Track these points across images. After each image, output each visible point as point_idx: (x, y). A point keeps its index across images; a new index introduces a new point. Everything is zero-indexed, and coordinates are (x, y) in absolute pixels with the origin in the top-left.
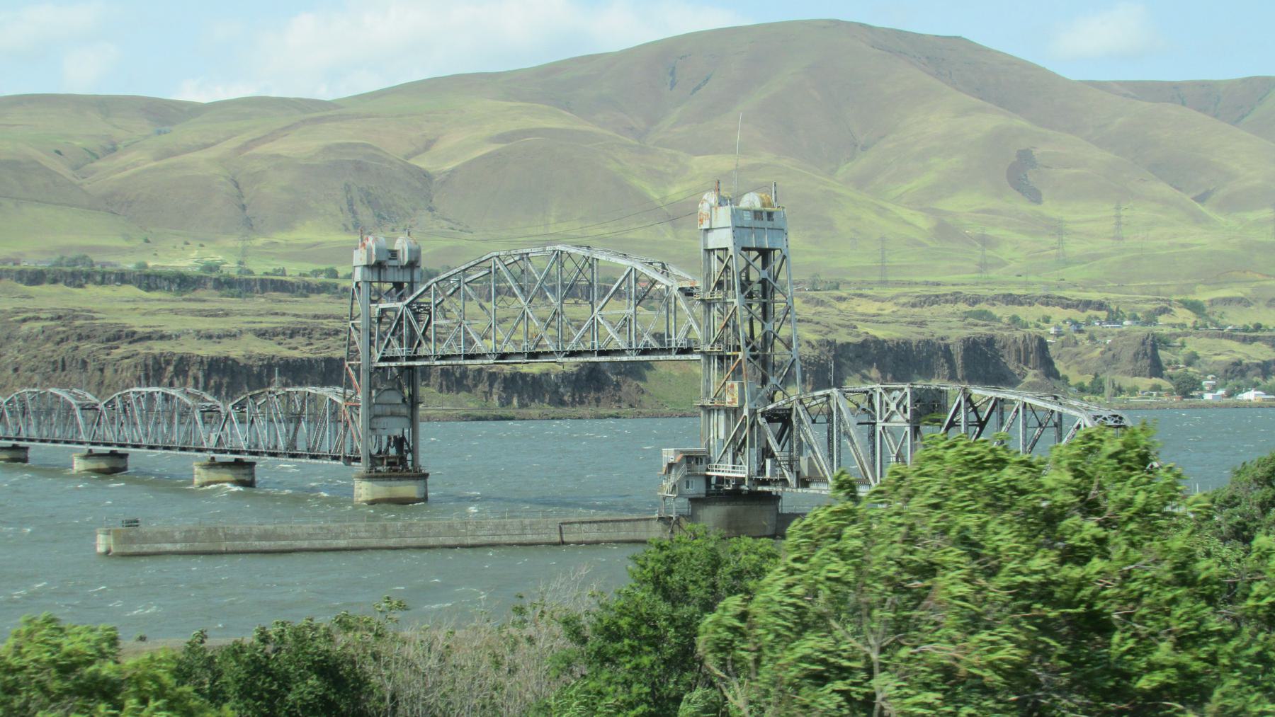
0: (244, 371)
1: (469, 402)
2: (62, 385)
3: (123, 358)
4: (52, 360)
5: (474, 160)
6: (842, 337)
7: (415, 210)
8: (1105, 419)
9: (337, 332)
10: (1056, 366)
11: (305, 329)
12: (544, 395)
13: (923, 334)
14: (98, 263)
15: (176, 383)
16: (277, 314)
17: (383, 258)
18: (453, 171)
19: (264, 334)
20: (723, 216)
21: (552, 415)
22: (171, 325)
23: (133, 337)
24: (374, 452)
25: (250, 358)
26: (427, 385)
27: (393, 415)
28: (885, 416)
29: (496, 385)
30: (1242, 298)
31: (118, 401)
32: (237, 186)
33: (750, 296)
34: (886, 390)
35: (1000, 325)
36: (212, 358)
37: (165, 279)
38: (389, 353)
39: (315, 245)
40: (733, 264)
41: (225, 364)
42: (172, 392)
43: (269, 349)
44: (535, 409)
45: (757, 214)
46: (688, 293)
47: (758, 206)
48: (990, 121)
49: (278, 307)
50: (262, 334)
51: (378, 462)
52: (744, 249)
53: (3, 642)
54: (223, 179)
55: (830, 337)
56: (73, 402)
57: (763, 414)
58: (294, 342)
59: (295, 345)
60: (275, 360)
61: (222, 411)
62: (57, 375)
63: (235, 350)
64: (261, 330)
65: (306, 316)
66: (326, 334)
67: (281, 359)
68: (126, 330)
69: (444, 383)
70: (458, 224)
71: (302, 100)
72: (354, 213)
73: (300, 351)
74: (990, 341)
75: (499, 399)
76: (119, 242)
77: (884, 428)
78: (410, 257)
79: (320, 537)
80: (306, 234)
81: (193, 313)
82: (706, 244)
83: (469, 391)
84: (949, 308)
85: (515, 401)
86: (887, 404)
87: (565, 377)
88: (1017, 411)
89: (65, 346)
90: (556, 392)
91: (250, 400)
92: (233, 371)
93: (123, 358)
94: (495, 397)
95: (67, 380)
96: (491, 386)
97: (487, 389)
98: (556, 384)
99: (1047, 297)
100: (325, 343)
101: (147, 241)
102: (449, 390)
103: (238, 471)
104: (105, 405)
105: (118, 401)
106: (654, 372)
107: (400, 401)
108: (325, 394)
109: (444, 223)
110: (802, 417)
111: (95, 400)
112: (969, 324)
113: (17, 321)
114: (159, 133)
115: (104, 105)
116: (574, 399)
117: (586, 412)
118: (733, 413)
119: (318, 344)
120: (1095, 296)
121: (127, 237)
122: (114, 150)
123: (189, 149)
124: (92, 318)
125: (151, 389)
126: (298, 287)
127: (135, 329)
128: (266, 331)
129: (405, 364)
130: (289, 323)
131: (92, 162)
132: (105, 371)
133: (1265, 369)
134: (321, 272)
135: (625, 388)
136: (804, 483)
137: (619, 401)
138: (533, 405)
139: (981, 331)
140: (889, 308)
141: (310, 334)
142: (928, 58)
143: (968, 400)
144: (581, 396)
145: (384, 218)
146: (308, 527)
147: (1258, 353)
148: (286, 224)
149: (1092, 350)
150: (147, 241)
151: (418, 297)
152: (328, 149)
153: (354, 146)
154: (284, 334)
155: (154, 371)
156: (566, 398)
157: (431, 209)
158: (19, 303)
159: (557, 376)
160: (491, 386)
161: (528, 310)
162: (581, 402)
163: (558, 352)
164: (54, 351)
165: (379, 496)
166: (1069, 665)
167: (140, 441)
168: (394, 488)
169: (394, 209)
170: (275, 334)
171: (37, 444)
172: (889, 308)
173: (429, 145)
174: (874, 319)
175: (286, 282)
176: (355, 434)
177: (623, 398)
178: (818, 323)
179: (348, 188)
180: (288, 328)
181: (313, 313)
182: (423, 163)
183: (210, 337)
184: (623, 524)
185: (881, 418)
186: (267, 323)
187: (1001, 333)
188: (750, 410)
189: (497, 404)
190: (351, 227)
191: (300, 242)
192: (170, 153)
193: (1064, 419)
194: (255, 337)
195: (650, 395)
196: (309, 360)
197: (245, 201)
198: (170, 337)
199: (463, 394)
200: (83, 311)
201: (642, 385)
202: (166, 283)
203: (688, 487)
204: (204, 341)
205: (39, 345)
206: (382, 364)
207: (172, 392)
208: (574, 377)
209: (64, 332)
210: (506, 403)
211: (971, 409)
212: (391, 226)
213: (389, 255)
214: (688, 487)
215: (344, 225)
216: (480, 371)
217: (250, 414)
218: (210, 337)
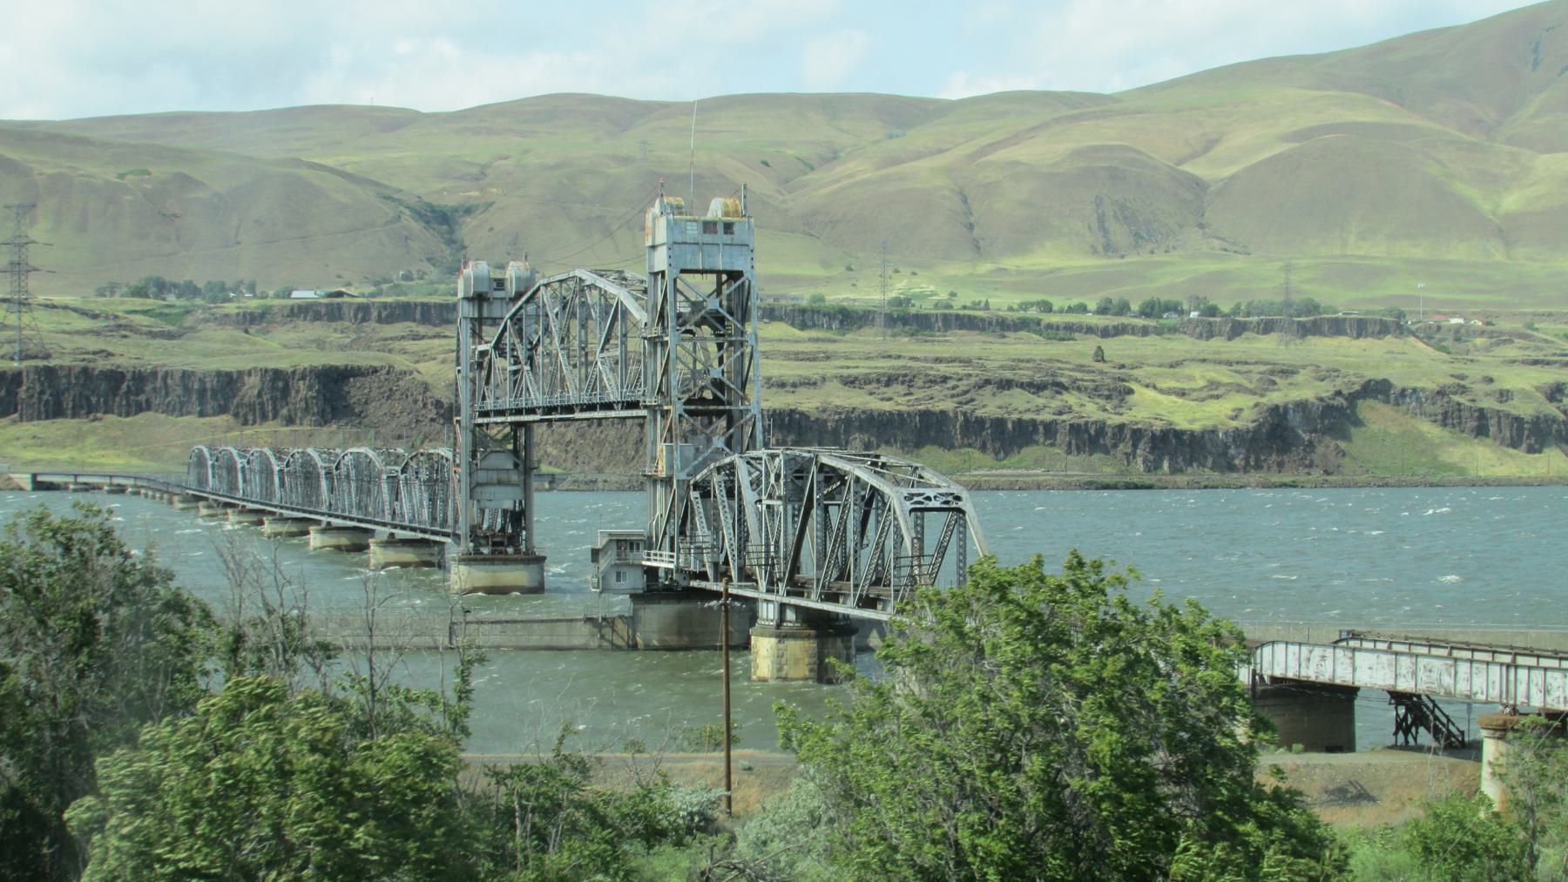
0: (816, 427)
1: (1104, 467)
5: (1259, 164)
7: (1181, 226)
9: (945, 379)
11: (905, 375)
12: (1206, 457)
14: (769, 296)
16: (890, 357)
17: (484, 289)
18: (1233, 178)
19: (852, 382)
21: (1203, 484)
25: (824, 411)
26: (1052, 445)
27: (500, 483)
29: (1141, 445)
32: (965, 201)
36: (774, 411)
37: (824, 315)
39: (1051, 272)
41: (791, 420)
44: (1192, 473)
50: (850, 382)
51: (483, 541)
54: (947, 193)
58: (889, 391)
60: (856, 413)
62: (592, 430)
64: (849, 376)
66: (931, 381)
67: (864, 412)
69: (1073, 442)
70: (1234, 243)
71: (1073, 93)
72: (1105, 231)
73: (896, 402)
75: (1144, 462)
76: (820, 272)
78: (517, 287)
80: (1044, 258)
82: (651, 267)
83: (1107, 452)
85: (1166, 465)
90: (1225, 454)
92: (800, 427)
94: (1140, 460)
95: (603, 436)
96: (1135, 446)
97: (1129, 450)
98: (1225, 444)
100: (929, 392)
101: (850, 269)
102: (1079, 450)
103: (422, 551)
106: (1364, 429)
107: (510, 466)
109: (1216, 243)
114: (891, 137)
115: (831, 106)
116: (1247, 463)
117: (1252, 480)
119: (919, 394)
121: (825, 264)
122: (834, 158)
123: (919, 156)
126: (990, 323)
128: (856, 378)
131: (805, 174)
134: (1032, 304)
135: (1320, 450)
137: (1311, 465)
138: (1190, 470)
141: (911, 381)
144: (1257, 460)
145: (1142, 238)
148: (1019, 248)
150: (850, 269)
152: (1077, 154)
153: (1111, 149)
154: (878, 381)
156: (1237, 462)
157: (1201, 226)
159: (1226, 433)
160: (1135, 446)
162: (1258, 467)
165: (479, 584)
168: (498, 574)
169: (1155, 226)
170: (868, 381)
173: (1210, 144)
175: (975, 317)
179: (1099, 202)
180: (884, 375)
182: (1197, 169)
183: (782, 385)
184: (536, 626)
190: (1100, 248)
191: (1032, 268)
192: (895, 161)
194: (840, 386)
195: (1353, 458)
196: (900, 414)
197: (972, 220)
199: (1097, 456)
201: (1343, 445)
202: (825, 320)
203: (618, 579)
204: (774, 390)
208: (1250, 435)
210: (1152, 467)
212: (1149, 247)
213: (495, 284)
214: (618, 579)
215: (1092, 246)
216: (1121, 427)
218: (782, 385)
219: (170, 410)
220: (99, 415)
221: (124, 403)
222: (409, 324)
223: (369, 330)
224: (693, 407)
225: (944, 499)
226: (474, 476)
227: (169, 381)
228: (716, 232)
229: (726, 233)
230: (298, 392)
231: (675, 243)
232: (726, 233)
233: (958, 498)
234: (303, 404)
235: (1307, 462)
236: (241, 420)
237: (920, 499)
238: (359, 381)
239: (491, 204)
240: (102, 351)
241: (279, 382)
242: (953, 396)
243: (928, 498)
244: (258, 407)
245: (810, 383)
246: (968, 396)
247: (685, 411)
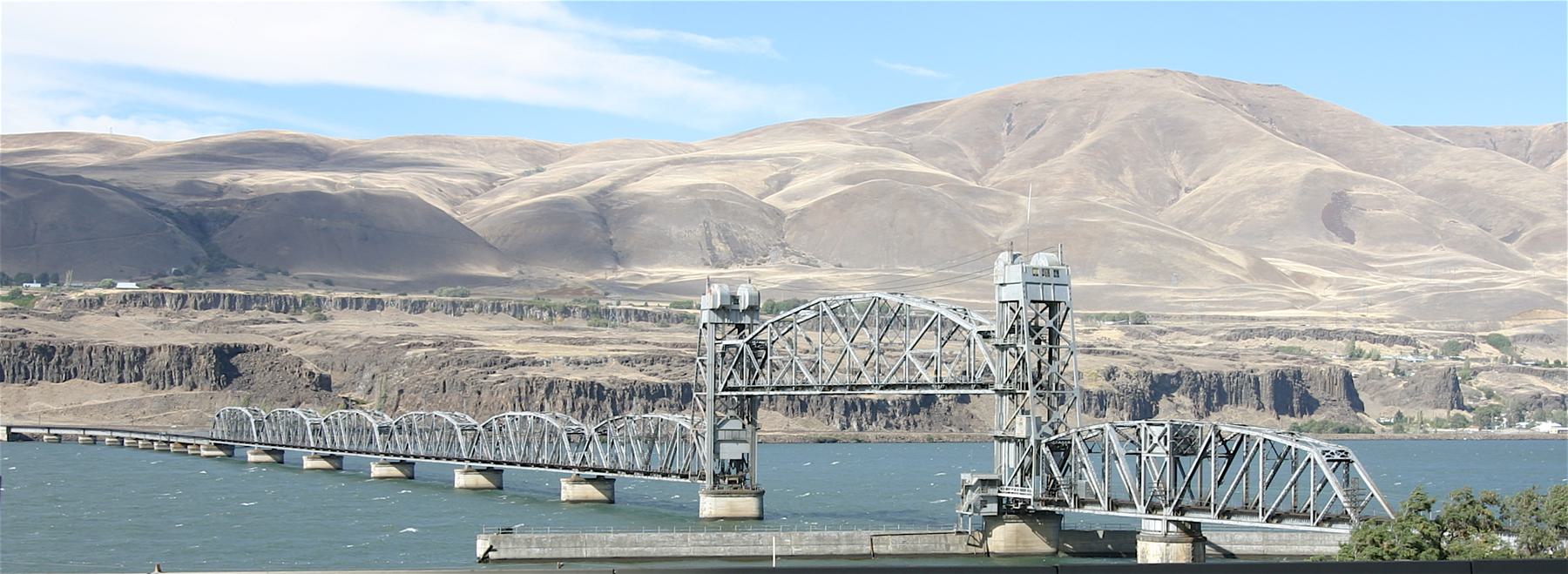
2: (444, 407)
3: (498, 382)
4: (435, 383)
6: (1158, 369)
8: (1332, 453)
10: (1361, 398)
11: (664, 357)
13: (1234, 366)
15: (547, 406)
16: (639, 342)
17: (727, 302)
20: (1015, 273)
23: (508, 363)
24: (717, 472)
28: (1149, 448)
30: (1544, 335)
31: (495, 422)
33: (1038, 342)
34: (1148, 424)
35: (1308, 359)
38: (731, 384)
39: (676, 278)
40: (1023, 314)
42: (542, 416)
43: (631, 375)
45: (1045, 272)
46: (986, 335)
47: (1046, 265)
48: (1301, 166)
49: (639, 336)
50: (626, 361)
52: (1033, 301)
55: (1146, 369)
56: (455, 423)
57: (1046, 444)
59: (655, 372)
60: (637, 385)
61: (586, 433)
63: (601, 376)
65: (666, 345)
67: (643, 384)
68: (501, 357)
73: (654, 377)
74: (1298, 375)
77: (1148, 457)
79: (666, 544)
81: (564, 341)
84: (1262, 342)
85: (854, 425)
86: (1151, 437)
87: (902, 403)
88: (1258, 445)
89: (446, 370)
91: (611, 424)
93: (498, 382)
94: (837, 421)
99: (1356, 332)
100: (683, 369)
104: (483, 427)
105: (495, 422)
108: (676, 420)
109: (794, 258)
110: (1080, 447)
111: (474, 422)
112: (1278, 357)
113: (402, 347)
118: (1021, 442)
119: (676, 371)
120: (1401, 331)
124: (471, 345)
125: (523, 414)
127: (511, 356)
129: (745, 393)
130: (650, 351)
132: (482, 394)
133: (1562, 400)
136: (1081, 503)
139: (1289, 364)
140: (1206, 341)
142: (1249, 105)
143: (1218, 434)
147: (1556, 388)
149: (1396, 383)
151: (757, 335)
155: (524, 395)
157: (783, 246)
158: (405, 330)
161: (850, 349)
163: (875, 386)
164: (435, 375)
166: (331, 467)
167: (514, 459)
171: (423, 460)
172: (1206, 341)
174: (1191, 352)
176: (701, 456)
177: (954, 422)
178: (1135, 355)
181: (673, 342)
185: (1145, 449)
186: (630, 351)
187: (1307, 367)
188: (1035, 440)
189: (838, 427)
193: (1299, 453)
200: (462, 338)
205: (423, 369)
206: (725, 393)
207: (542, 416)
209: (446, 357)
211: (1220, 444)
217: (611, 436)
219: (92, 376)
221: (56, 370)
223: (188, 314)
227: (93, 354)
230: (199, 364)
231: (1027, 283)
234: (204, 374)
235: (948, 423)
236: (153, 384)
237: (1329, 454)
238: (252, 356)
239: (237, 217)
241: (184, 357)
244: (166, 375)
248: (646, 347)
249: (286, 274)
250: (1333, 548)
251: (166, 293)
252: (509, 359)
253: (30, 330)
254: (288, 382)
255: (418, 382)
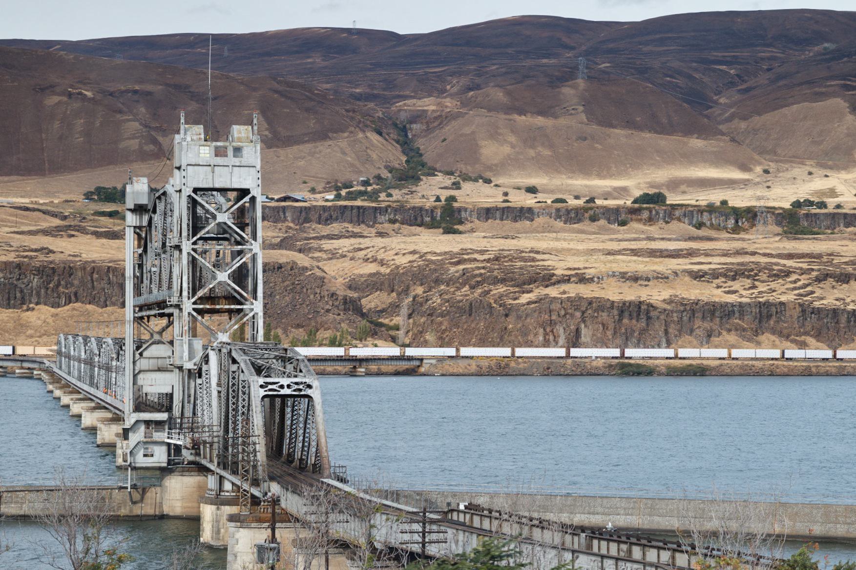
16: (746, 253)
22: (596, 266)
36: (624, 303)
50: (698, 276)
53: (220, 553)
58: (736, 285)
64: (700, 271)
66: (775, 275)
100: (773, 285)
119: (762, 287)
121: (744, 168)
124: (533, 260)
127: (556, 272)
146: (633, 493)
154: (725, 276)
198: (591, 280)
204: (628, 283)
220: (31, 306)
222: (346, 225)
224: (201, 306)
225: (296, 387)
226: (138, 363)
228: (226, 156)
229: (234, 156)
232: (234, 156)
233: (310, 387)
237: (274, 387)
240: (43, 249)
242: (795, 289)
243: (282, 387)
245: (662, 278)
246: (809, 289)
247: (194, 309)
248: (109, 255)
249: (488, 181)
250: (597, 516)
251: (288, 206)
252: (554, 275)
253: (55, 250)
254: (307, 306)
255: (447, 304)
